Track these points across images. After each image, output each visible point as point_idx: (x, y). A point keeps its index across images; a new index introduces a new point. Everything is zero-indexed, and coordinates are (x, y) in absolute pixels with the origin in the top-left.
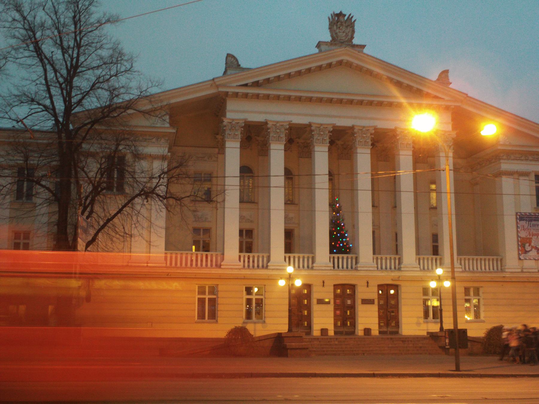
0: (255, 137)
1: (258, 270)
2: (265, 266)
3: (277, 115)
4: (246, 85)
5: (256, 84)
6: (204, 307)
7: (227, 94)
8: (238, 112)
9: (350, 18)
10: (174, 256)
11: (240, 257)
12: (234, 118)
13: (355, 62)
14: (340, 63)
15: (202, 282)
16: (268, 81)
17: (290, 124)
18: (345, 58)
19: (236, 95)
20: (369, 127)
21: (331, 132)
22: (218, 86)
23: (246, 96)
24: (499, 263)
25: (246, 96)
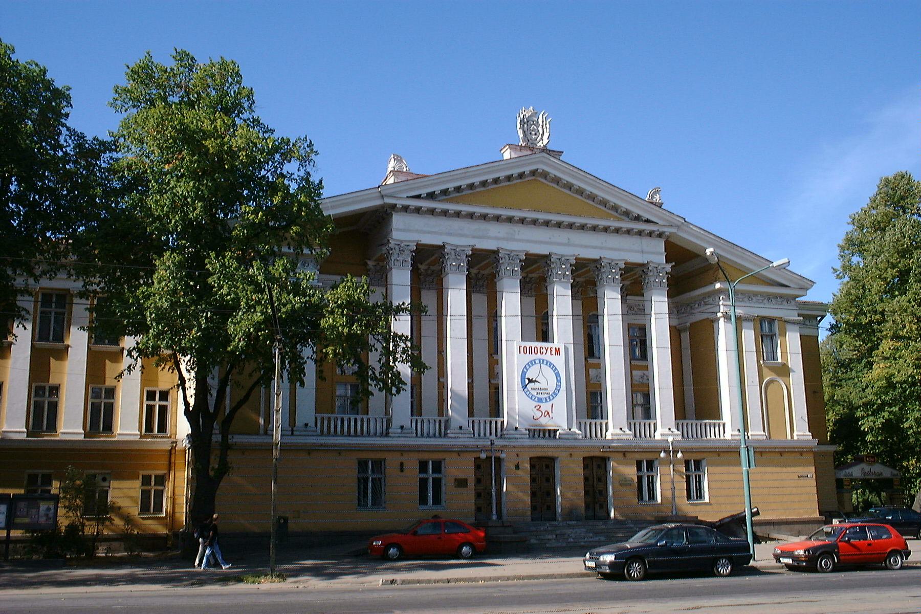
0: (428, 266)
1: (439, 439)
2: (384, 432)
3: (459, 236)
4: (418, 197)
5: (431, 196)
6: (366, 488)
7: (394, 206)
8: (406, 231)
9: (223, 65)
10: (717, 436)
11: (316, 418)
12: (402, 239)
13: (553, 172)
14: (534, 173)
15: (425, 456)
16: (445, 192)
17: (417, 245)
18: (541, 167)
19: (406, 209)
20: (520, 251)
21: (470, 256)
22: (382, 197)
23: (418, 210)
24: (721, 428)
25: (418, 210)
